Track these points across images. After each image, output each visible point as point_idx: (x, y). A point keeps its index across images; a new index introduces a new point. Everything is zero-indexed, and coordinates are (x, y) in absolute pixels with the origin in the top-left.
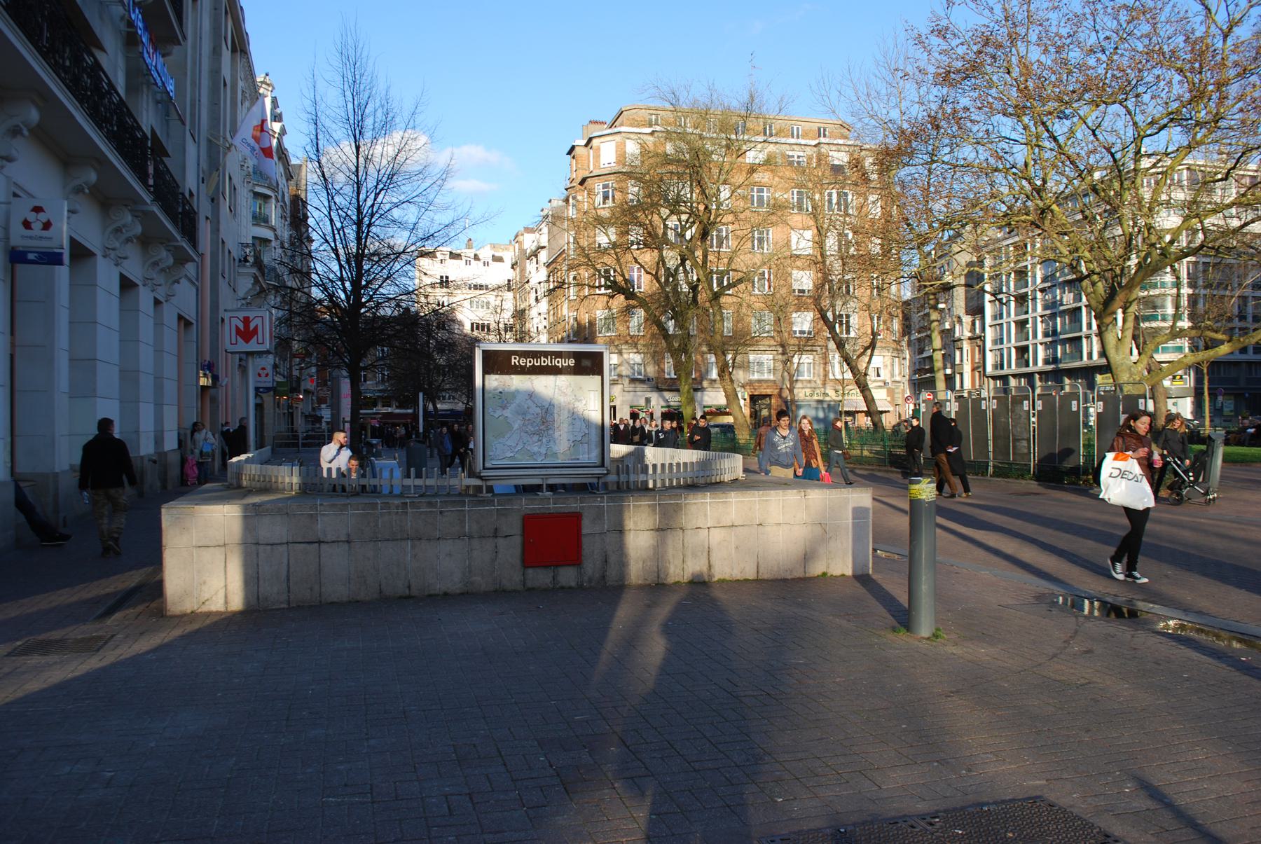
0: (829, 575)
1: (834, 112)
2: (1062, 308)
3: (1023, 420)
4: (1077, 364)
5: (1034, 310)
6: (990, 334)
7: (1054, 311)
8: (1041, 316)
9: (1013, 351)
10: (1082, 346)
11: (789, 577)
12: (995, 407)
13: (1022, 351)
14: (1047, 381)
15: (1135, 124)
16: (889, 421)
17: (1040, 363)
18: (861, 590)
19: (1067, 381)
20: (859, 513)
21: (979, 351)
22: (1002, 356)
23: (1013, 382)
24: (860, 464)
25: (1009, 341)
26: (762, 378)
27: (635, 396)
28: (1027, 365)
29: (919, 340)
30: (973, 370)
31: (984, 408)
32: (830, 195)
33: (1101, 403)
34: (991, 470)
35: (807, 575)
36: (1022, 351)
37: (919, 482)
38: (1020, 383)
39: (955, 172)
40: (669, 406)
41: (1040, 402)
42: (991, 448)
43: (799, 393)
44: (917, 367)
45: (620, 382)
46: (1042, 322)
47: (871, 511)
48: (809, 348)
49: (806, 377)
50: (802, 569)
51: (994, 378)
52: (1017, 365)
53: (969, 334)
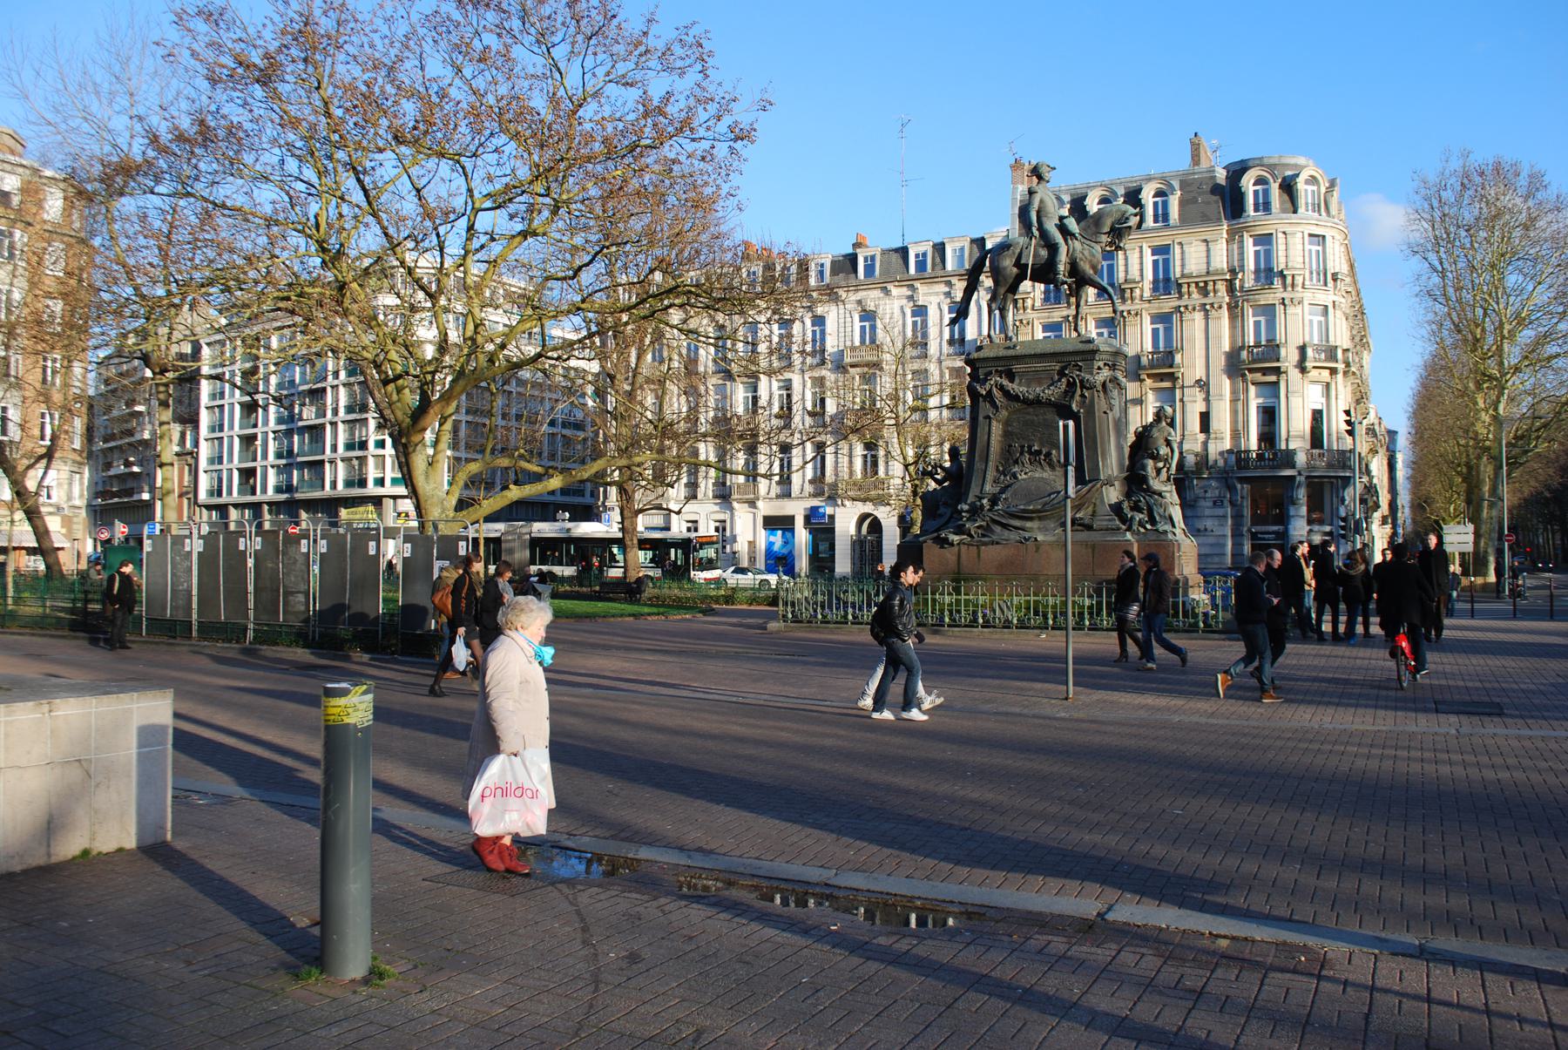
0: (94, 853)
1: (27, 97)
2: (301, 424)
3: (300, 566)
4: (317, 494)
5: (266, 423)
6: (205, 451)
7: (290, 426)
8: (274, 432)
9: (236, 474)
10: (324, 473)
11: (18, 868)
12: (258, 547)
13: (248, 474)
14: (278, 514)
15: (470, 191)
16: (68, 563)
17: (270, 491)
18: (171, 884)
19: (304, 515)
20: (148, 735)
21: (190, 471)
22: (220, 480)
23: (234, 514)
24: (42, 628)
25: (231, 460)
28: (254, 493)
29: (103, 451)
31: (242, 547)
33: (409, 545)
34: (250, 634)
35: (54, 860)
36: (248, 474)
37: (344, 693)
38: (243, 515)
41: (324, 542)
42: (251, 605)
44: (100, 488)
46: (275, 439)
47: (171, 731)
50: (43, 850)
51: (209, 507)
52: (239, 493)
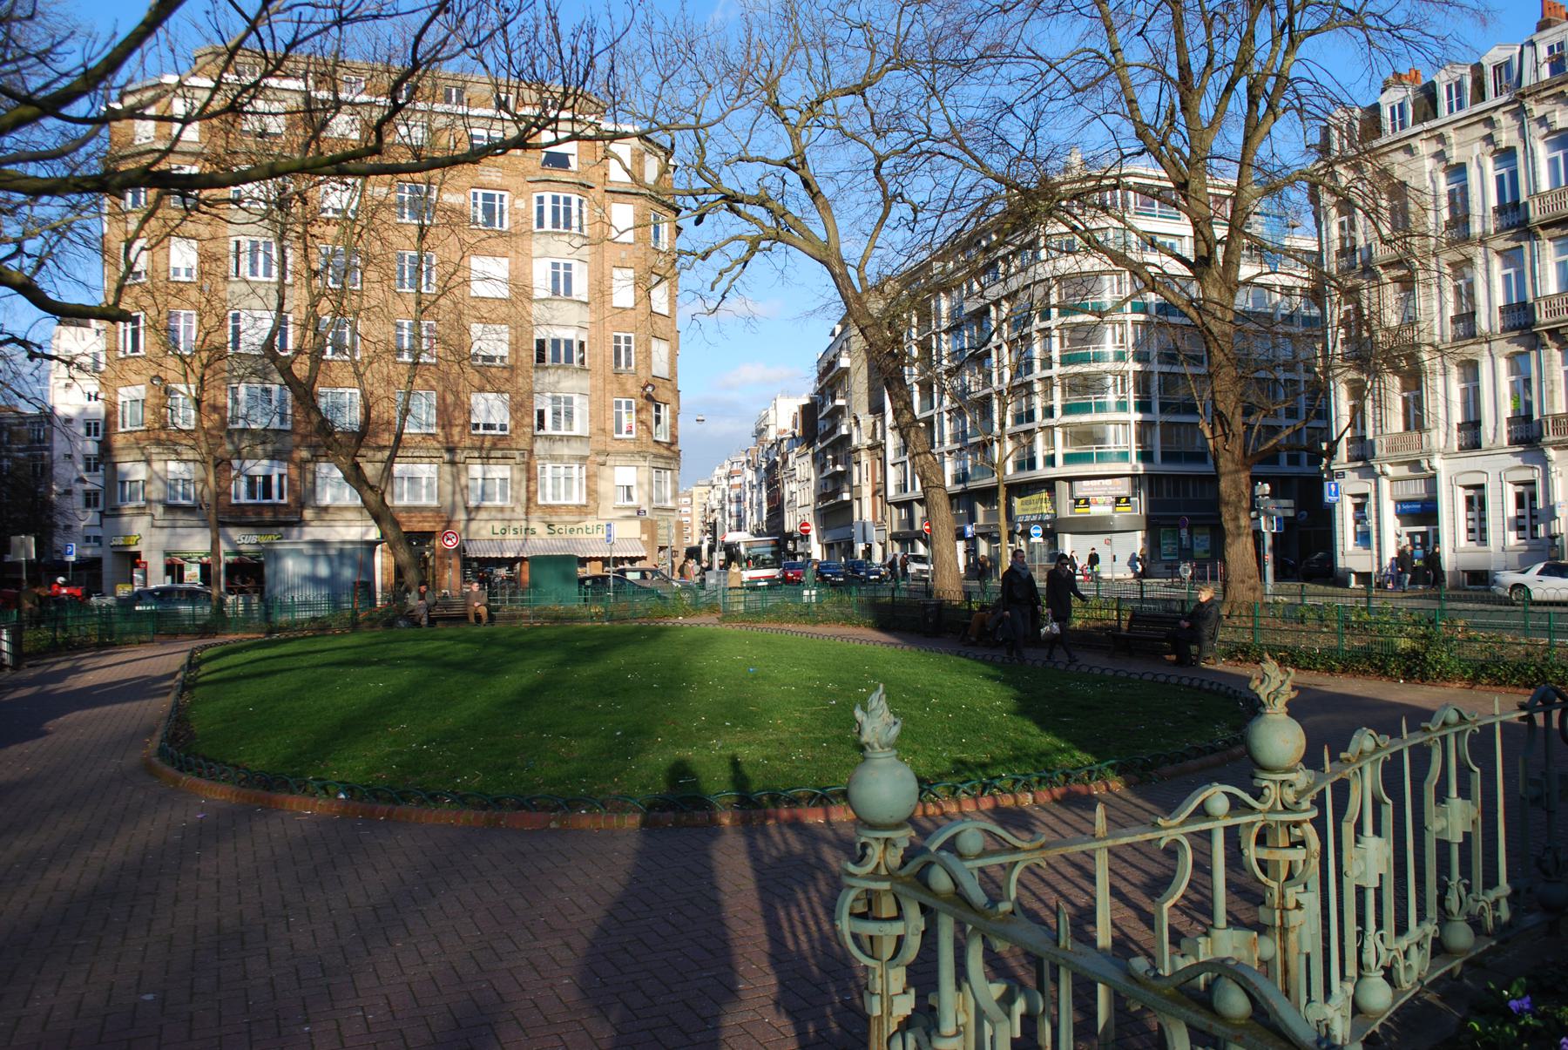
19: (980, 509)
26: (417, 503)
27: (172, 535)
30: (874, 494)
32: (541, 199)
39: (1291, 306)
40: (238, 553)
43: (479, 529)
45: (148, 511)
48: (499, 454)
49: (498, 502)
51: (898, 505)
53: (870, 442)
